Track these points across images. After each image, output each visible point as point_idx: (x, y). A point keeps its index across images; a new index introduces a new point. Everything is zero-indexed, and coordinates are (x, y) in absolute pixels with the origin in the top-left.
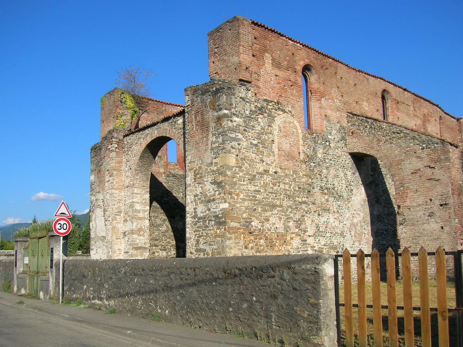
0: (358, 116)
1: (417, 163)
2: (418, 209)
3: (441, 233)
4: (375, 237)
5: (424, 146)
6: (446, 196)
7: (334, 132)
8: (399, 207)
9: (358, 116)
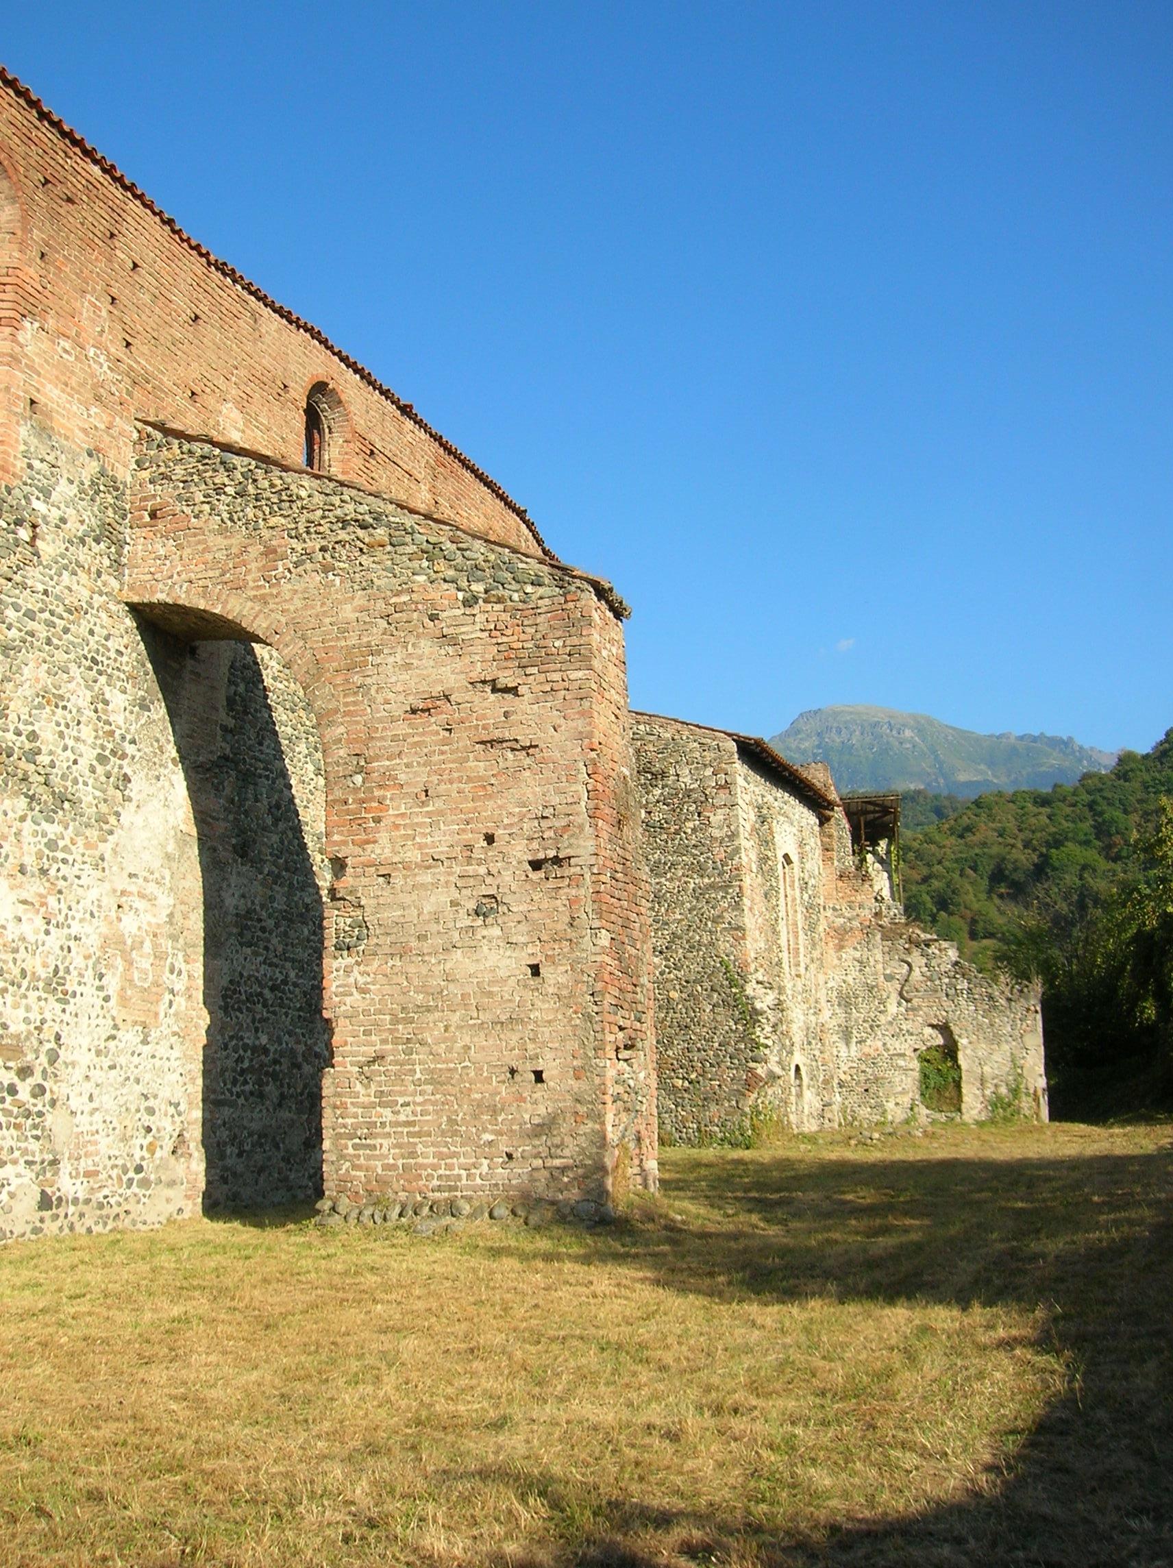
0: (190, 439)
1: (438, 664)
2: (427, 878)
3: (528, 995)
4: (221, 1014)
5: (478, 588)
6: (560, 823)
7: (64, 490)
8: (339, 866)
9: (190, 439)
